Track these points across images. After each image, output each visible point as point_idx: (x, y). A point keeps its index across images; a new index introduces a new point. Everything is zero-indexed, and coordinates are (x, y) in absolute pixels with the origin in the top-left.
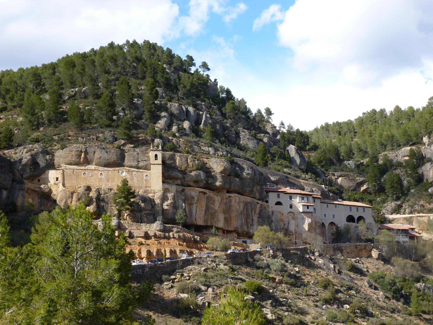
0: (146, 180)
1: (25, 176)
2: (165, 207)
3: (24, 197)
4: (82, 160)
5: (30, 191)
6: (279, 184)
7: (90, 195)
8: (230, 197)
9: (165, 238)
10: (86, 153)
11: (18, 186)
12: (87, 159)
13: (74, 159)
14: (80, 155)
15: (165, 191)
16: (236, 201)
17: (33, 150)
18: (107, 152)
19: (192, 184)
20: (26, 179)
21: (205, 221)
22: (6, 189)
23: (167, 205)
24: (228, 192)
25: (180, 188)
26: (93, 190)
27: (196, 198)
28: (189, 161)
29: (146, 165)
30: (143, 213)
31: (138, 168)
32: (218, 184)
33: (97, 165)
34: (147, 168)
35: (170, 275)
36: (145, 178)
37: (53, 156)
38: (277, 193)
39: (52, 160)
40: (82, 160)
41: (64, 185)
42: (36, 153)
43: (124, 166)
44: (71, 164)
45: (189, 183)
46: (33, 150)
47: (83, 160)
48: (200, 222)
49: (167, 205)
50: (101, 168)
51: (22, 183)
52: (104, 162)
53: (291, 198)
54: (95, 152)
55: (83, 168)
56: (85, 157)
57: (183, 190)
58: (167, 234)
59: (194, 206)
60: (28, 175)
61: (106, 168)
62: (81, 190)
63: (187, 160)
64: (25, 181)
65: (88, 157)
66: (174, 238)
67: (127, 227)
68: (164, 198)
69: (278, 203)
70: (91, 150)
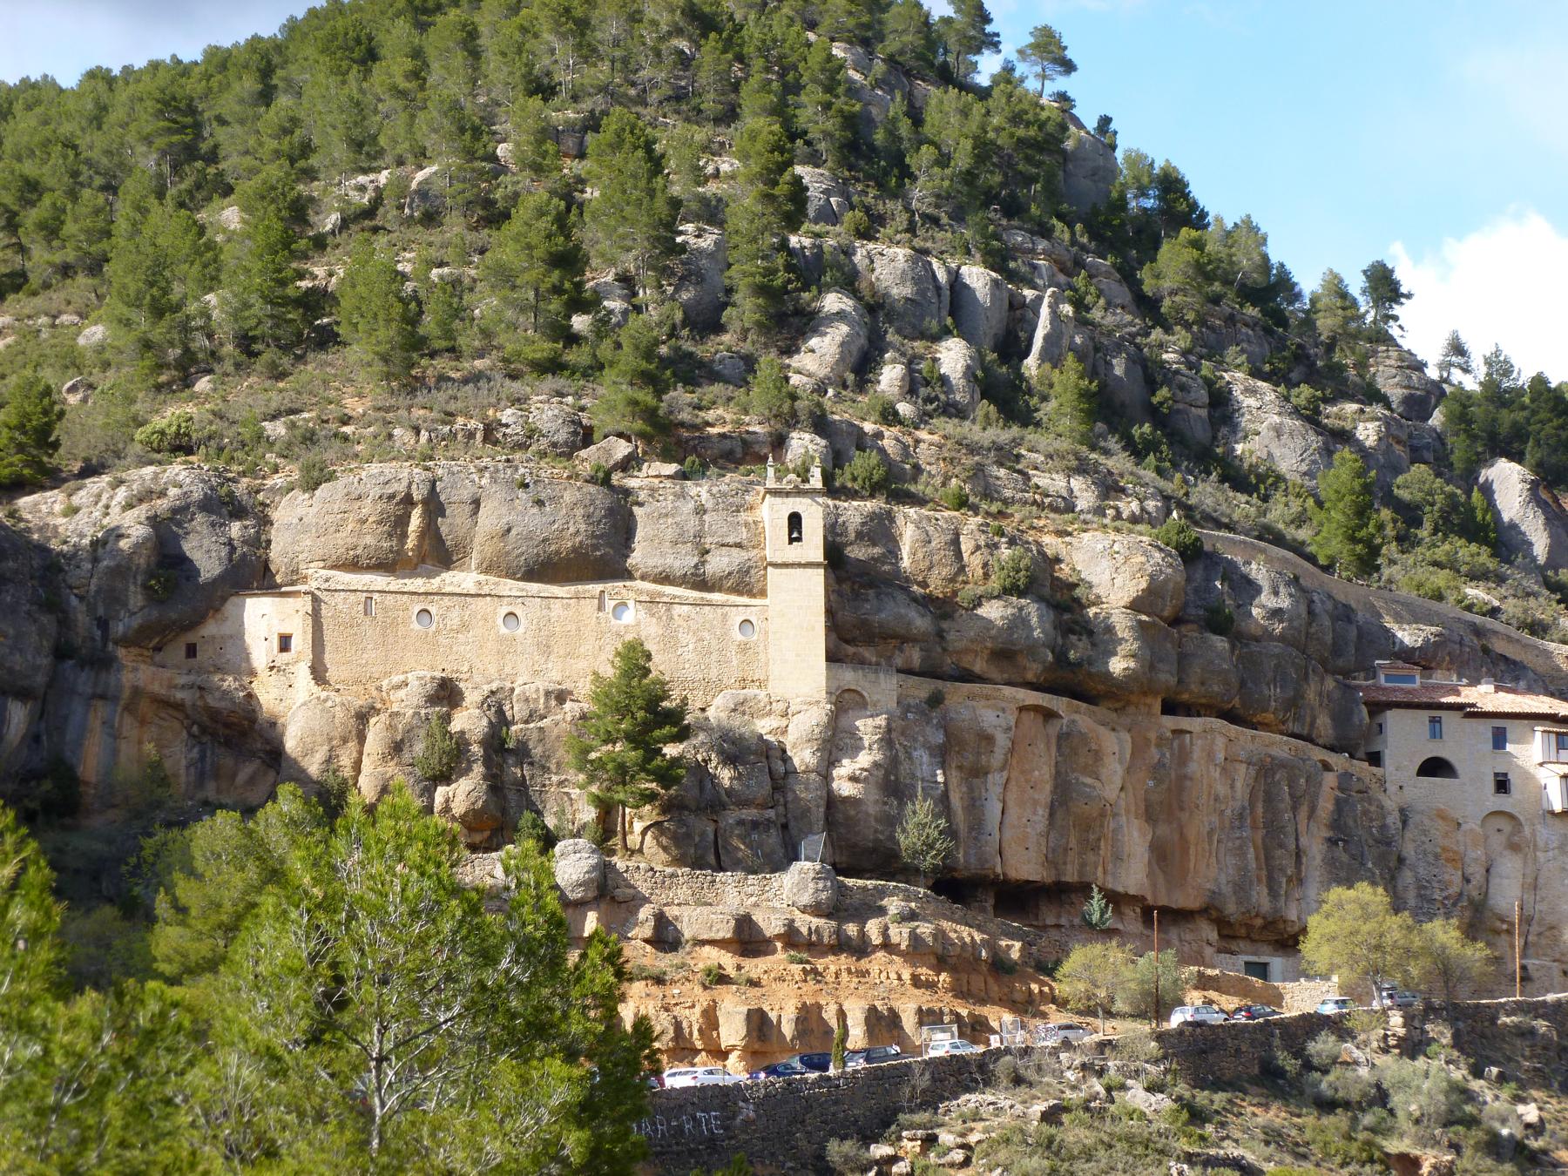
0: (744, 648)
1: (119, 629)
2: (844, 788)
3: (115, 735)
4: (411, 543)
5: (144, 706)
6: (1439, 666)
7: (455, 726)
8: (1178, 732)
9: (841, 946)
10: (434, 507)
11: (84, 681)
12: (439, 540)
13: (369, 540)
14: (402, 521)
15: (844, 703)
16: (1210, 756)
17: (163, 494)
18: (540, 503)
19: (979, 666)
20: (126, 642)
21: (1050, 861)
22: (23, 694)
23: (853, 779)
24: (1170, 708)
25: (921, 689)
26: (472, 697)
27: (1002, 741)
28: (966, 545)
29: (745, 571)
30: (732, 816)
31: (700, 582)
32: (1118, 665)
33: (488, 568)
34: (745, 583)
35: (868, 1139)
36: (738, 636)
37: (265, 522)
38: (1425, 715)
39: (260, 543)
40: (411, 543)
41: (319, 673)
42: (175, 511)
43: (627, 575)
44: (353, 566)
45: (967, 661)
46: (163, 494)
47: (419, 547)
48: (1025, 865)
49: (853, 779)
50: (510, 586)
51: (102, 662)
52: (526, 552)
53: (1499, 740)
54: (476, 503)
55: (417, 584)
56: (430, 530)
57: (936, 700)
58: (851, 929)
59: (995, 780)
60: (136, 622)
61: (534, 587)
62: (407, 700)
63: (955, 542)
64: (121, 652)
65: (444, 526)
66: (887, 946)
67: (644, 888)
68: (835, 742)
69: (1435, 767)
70: (455, 494)
